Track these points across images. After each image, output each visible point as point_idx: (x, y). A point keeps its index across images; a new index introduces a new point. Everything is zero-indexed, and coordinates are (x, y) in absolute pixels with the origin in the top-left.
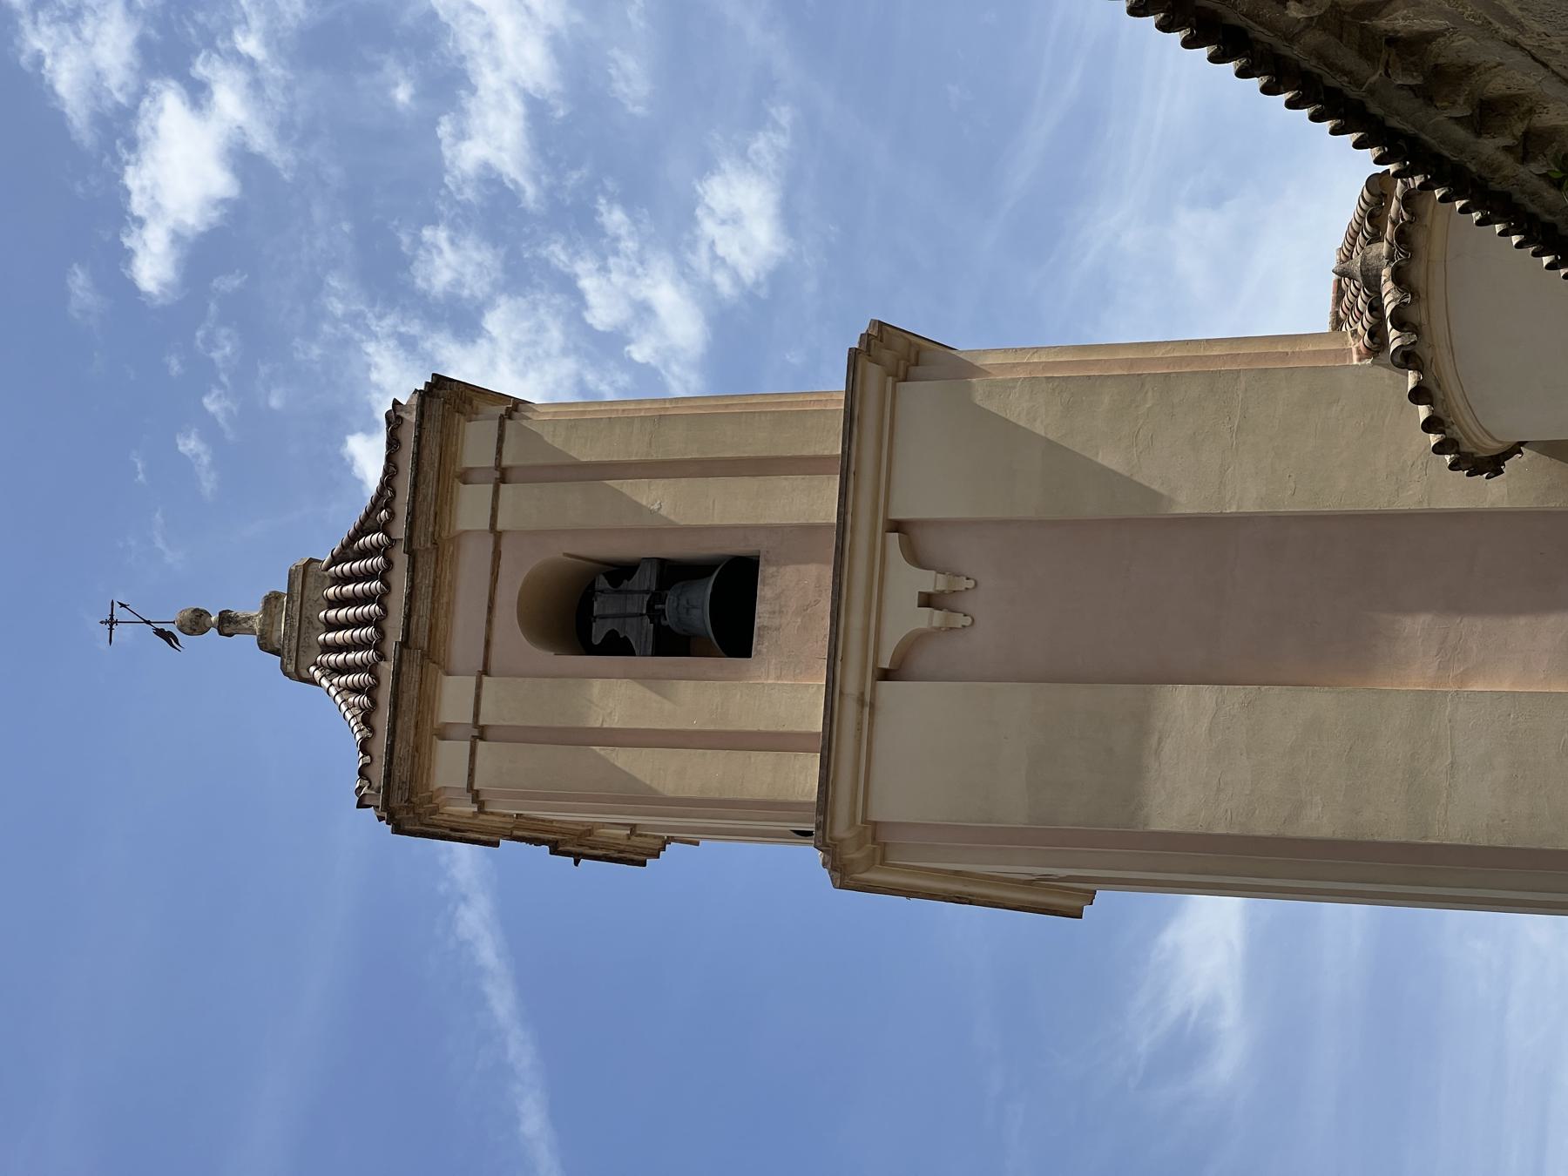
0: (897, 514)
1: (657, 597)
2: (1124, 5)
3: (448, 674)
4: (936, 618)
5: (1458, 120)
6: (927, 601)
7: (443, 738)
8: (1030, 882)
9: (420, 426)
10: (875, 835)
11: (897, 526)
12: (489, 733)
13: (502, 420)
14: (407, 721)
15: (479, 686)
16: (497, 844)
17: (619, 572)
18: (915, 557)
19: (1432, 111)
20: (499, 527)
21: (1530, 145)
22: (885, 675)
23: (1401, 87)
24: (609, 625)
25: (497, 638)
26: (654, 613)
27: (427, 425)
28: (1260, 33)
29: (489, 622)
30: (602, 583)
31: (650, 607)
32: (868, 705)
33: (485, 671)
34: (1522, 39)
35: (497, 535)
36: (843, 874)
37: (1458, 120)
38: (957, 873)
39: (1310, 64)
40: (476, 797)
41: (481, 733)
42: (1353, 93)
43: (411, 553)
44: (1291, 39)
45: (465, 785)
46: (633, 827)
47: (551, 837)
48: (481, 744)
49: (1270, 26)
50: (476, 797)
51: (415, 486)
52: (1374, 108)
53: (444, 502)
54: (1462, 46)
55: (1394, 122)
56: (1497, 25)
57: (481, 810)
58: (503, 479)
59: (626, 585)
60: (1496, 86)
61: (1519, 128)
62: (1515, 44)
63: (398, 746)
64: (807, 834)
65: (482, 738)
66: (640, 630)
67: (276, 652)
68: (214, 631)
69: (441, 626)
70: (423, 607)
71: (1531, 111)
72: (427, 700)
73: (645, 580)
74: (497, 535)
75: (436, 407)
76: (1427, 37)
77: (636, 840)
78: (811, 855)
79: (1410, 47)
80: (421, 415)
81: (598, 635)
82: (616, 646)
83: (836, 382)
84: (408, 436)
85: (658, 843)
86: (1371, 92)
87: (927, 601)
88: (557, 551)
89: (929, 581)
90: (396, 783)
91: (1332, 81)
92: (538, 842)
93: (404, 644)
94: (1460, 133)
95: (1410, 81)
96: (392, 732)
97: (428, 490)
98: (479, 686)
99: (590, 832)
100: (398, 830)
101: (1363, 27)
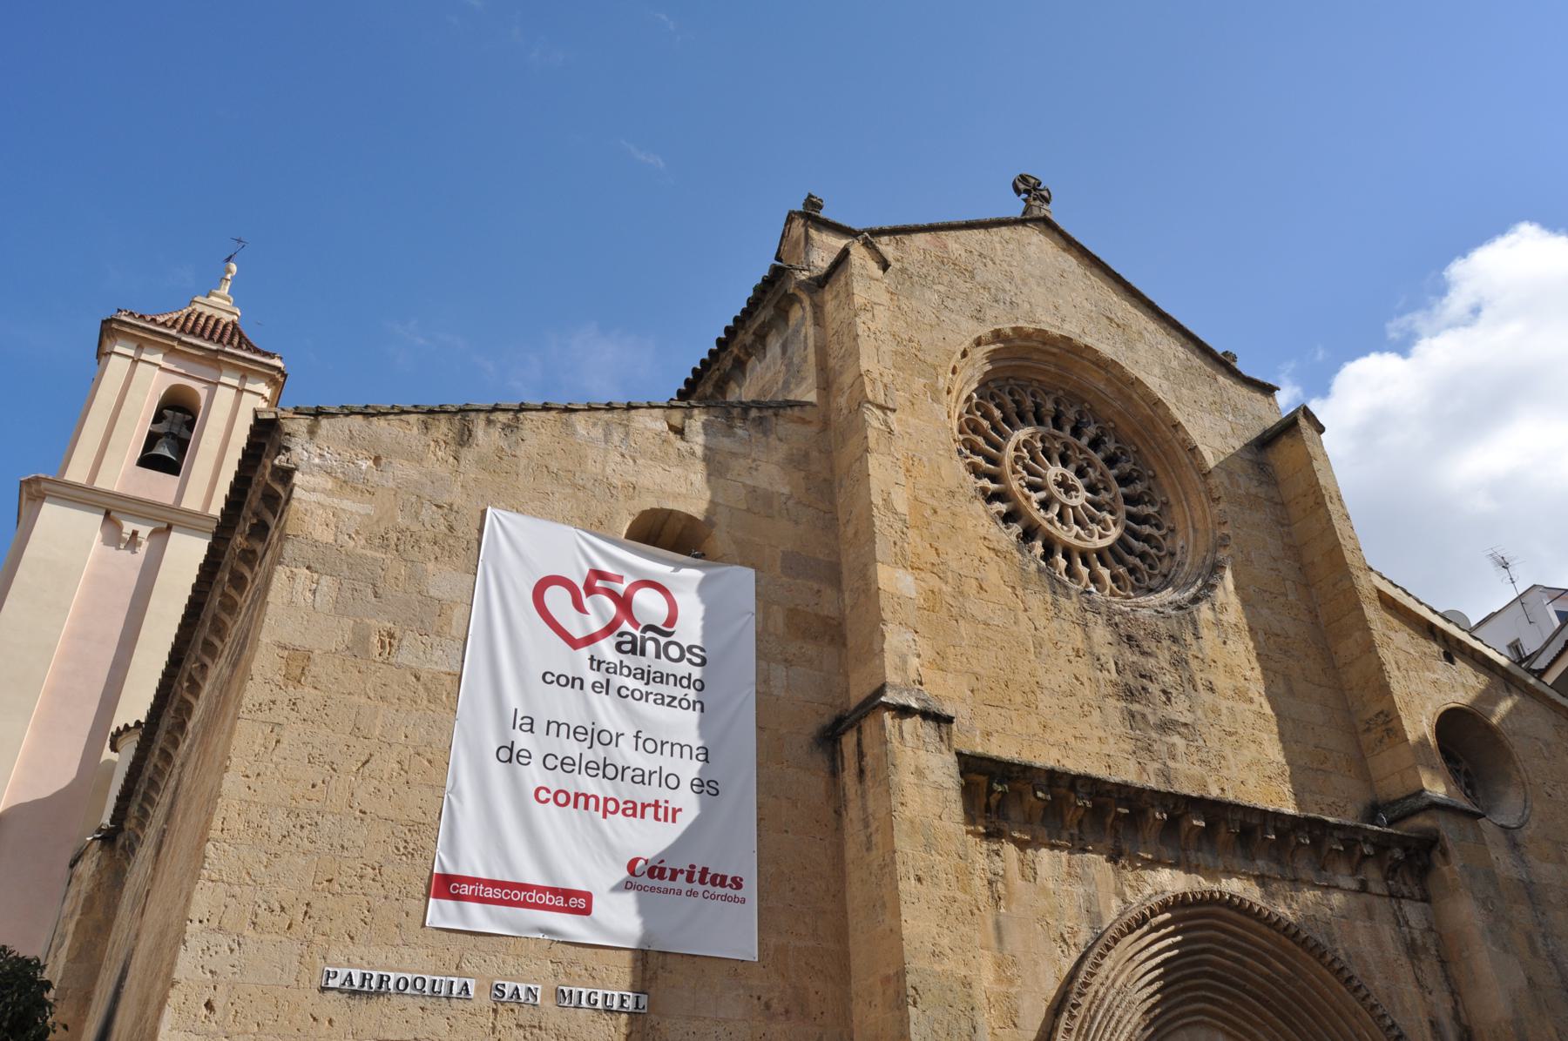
17: (190, 425)
73: (184, 433)
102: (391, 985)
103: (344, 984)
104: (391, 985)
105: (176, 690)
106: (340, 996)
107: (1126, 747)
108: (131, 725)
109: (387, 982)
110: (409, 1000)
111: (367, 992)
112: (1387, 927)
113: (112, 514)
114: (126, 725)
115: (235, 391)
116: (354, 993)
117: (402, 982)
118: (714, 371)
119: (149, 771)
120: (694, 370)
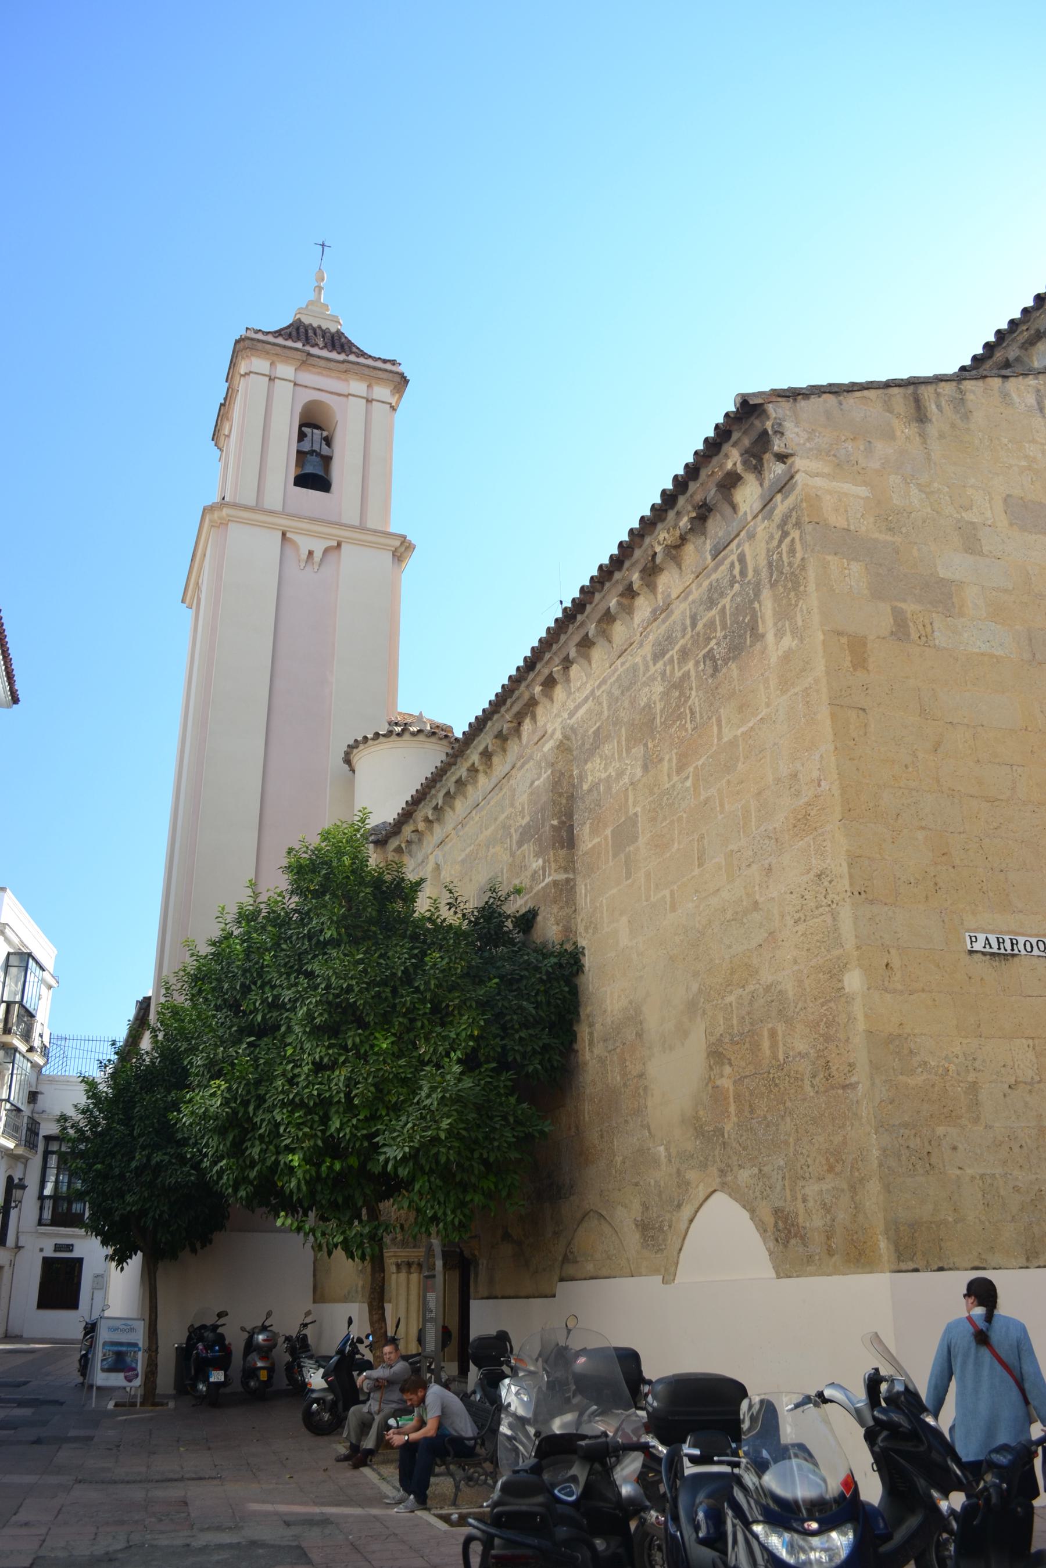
0: (343, 545)
1: (318, 454)
2: (1042, 291)
3: (296, 370)
4: (304, 554)
5: (487, 747)
6: (311, 553)
7: (271, 364)
8: (198, 583)
9: (391, 372)
10: (223, 524)
11: (339, 545)
12: (272, 382)
13: (391, 404)
14: (278, 350)
15: (290, 381)
16: (227, 381)
17: (328, 441)
18: (326, 551)
19: (492, 737)
20: (350, 397)
21: (473, 770)
22: (284, 534)
23: (503, 727)
24: (309, 435)
25: (308, 391)
26: (312, 452)
27: (391, 375)
28: (531, 675)
29: (315, 389)
30: (325, 434)
31: (314, 451)
32: (271, 527)
33: (295, 384)
34: (515, 769)
35: (347, 396)
36: (207, 510)
37: (487, 747)
38: (205, 555)
39: (517, 693)
40: (247, 374)
41: (271, 379)
42: (503, 709)
43: (343, 362)
44: (528, 687)
45: (252, 370)
46: (228, 436)
47: (227, 404)
48: (267, 378)
49: (533, 680)
50: (247, 374)
51: (368, 366)
52: (496, 717)
53: (362, 377)
54: (514, 748)
55: (489, 724)
56: (522, 761)
57: (242, 375)
58: (368, 401)
59: (324, 443)
60: (495, 760)
61: (481, 768)
62: (513, 767)
63: (269, 346)
64: (223, 499)
65: (270, 379)
66: (306, 446)
67: (307, 306)
68: (316, 284)
69: (314, 370)
70: (322, 363)
71: (486, 773)
72: (286, 360)
73: (325, 450)
74: (347, 396)
75: (397, 379)
76: (519, 737)
77: (222, 438)
78: (216, 499)
79: (517, 730)
80: (397, 373)
81: (305, 429)
82: (302, 436)
83: (394, 528)
84: (388, 366)
85: (221, 445)
86: (503, 716)
87: (311, 553)
88: (339, 417)
89: (318, 555)
90: (255, 343)
91: (509, 702)
92: (225, 399)
93: (309, 354)
94: (481, 748)
95: (504, 730)
96: (274, 344)
97: (366, 371)
98: (290, 381)
99: (228, 419)
100: (237, 342)
101: (527, 714)
102: (1021, 946)
103: (985, 947)
104: (1021, 946)
105: (521, 694)
106: (984, 958)
107: (735, 673)
108: (360, 739)
109: (1017, 944)
110: (1036, 961)
111: (1004, 955)
112: (774, 1538)
113: (288, 535)
114: (356, 741)
115: (365, 401)
116: (993, 954)
117: (1028, 944)
118: (1022, 332)
119: (449, 782)
120: (999, 333)
